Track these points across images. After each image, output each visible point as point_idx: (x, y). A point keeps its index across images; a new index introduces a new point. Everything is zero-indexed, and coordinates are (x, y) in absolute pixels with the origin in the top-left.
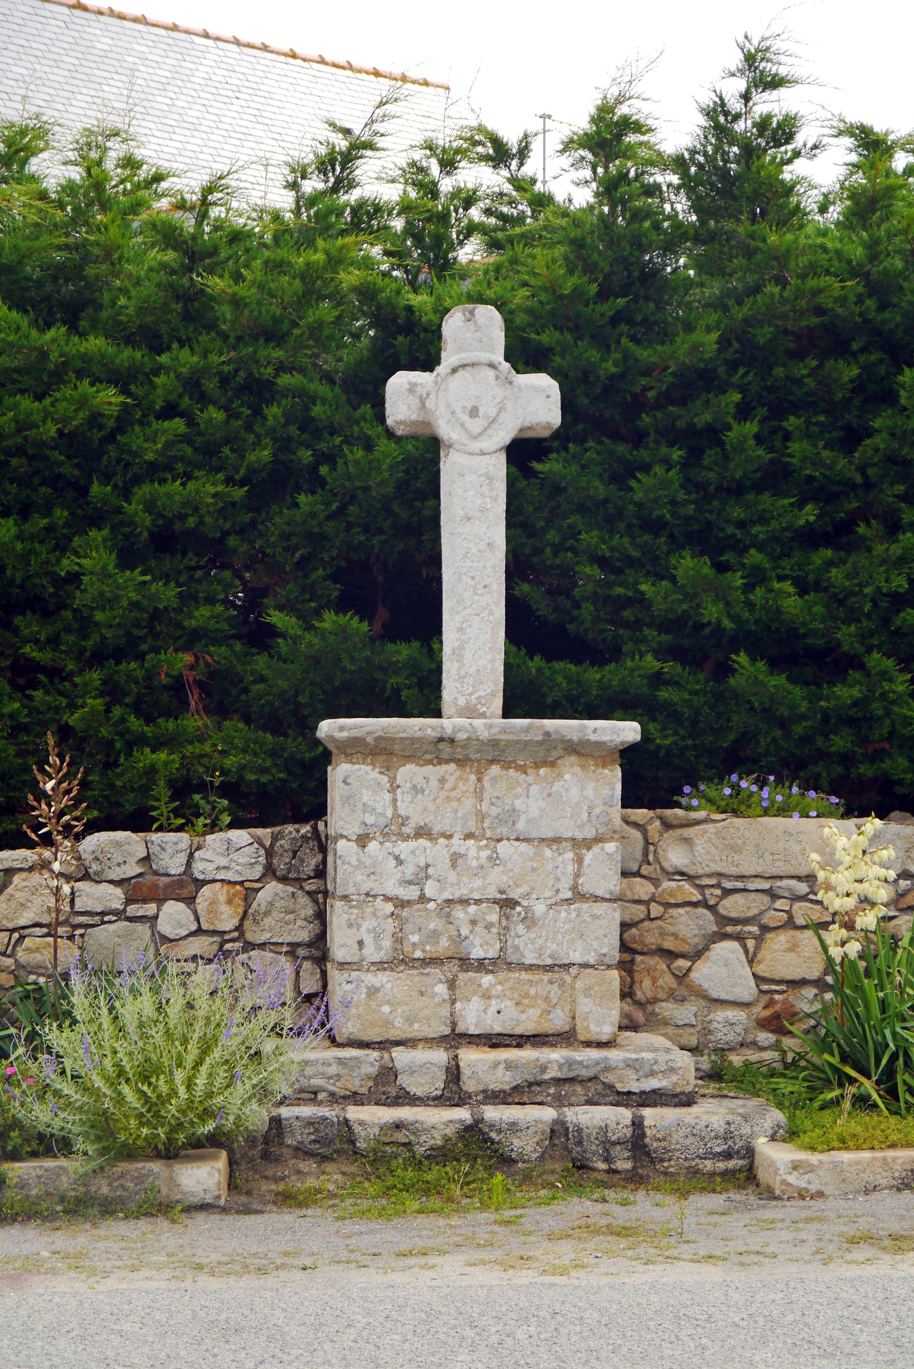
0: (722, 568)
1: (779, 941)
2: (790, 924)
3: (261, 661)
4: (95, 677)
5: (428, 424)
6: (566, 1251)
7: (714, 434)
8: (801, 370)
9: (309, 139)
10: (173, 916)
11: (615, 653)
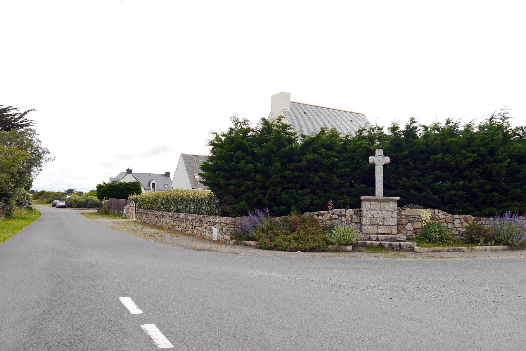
0: (409, 179)
1: (416, 223)
2: (417, 221)
3: (353, 190)
4: (334, 191)
6: (394, 257)
7: (408, 163)
8: (418, 155)
9: (357, 129)
10: (343, 219)
11: (395, 189)
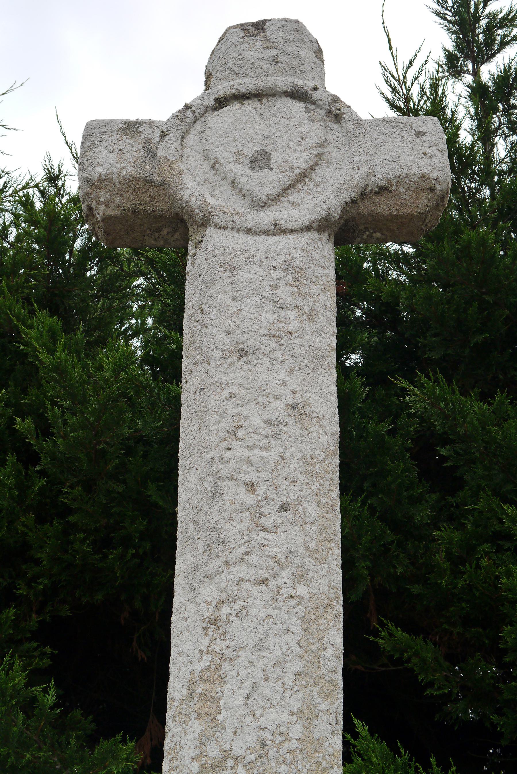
5: (161, 186)
